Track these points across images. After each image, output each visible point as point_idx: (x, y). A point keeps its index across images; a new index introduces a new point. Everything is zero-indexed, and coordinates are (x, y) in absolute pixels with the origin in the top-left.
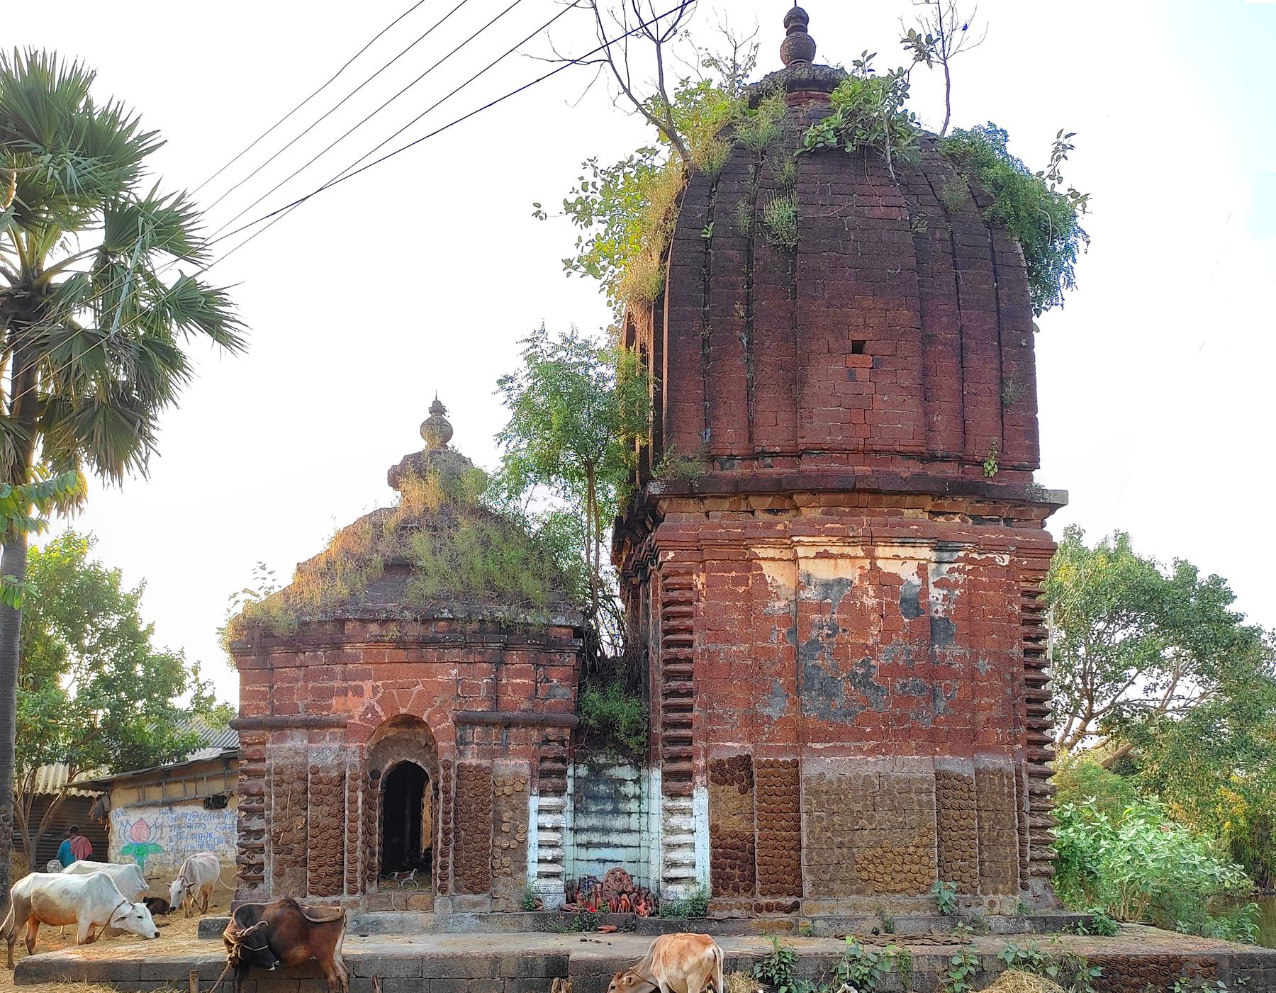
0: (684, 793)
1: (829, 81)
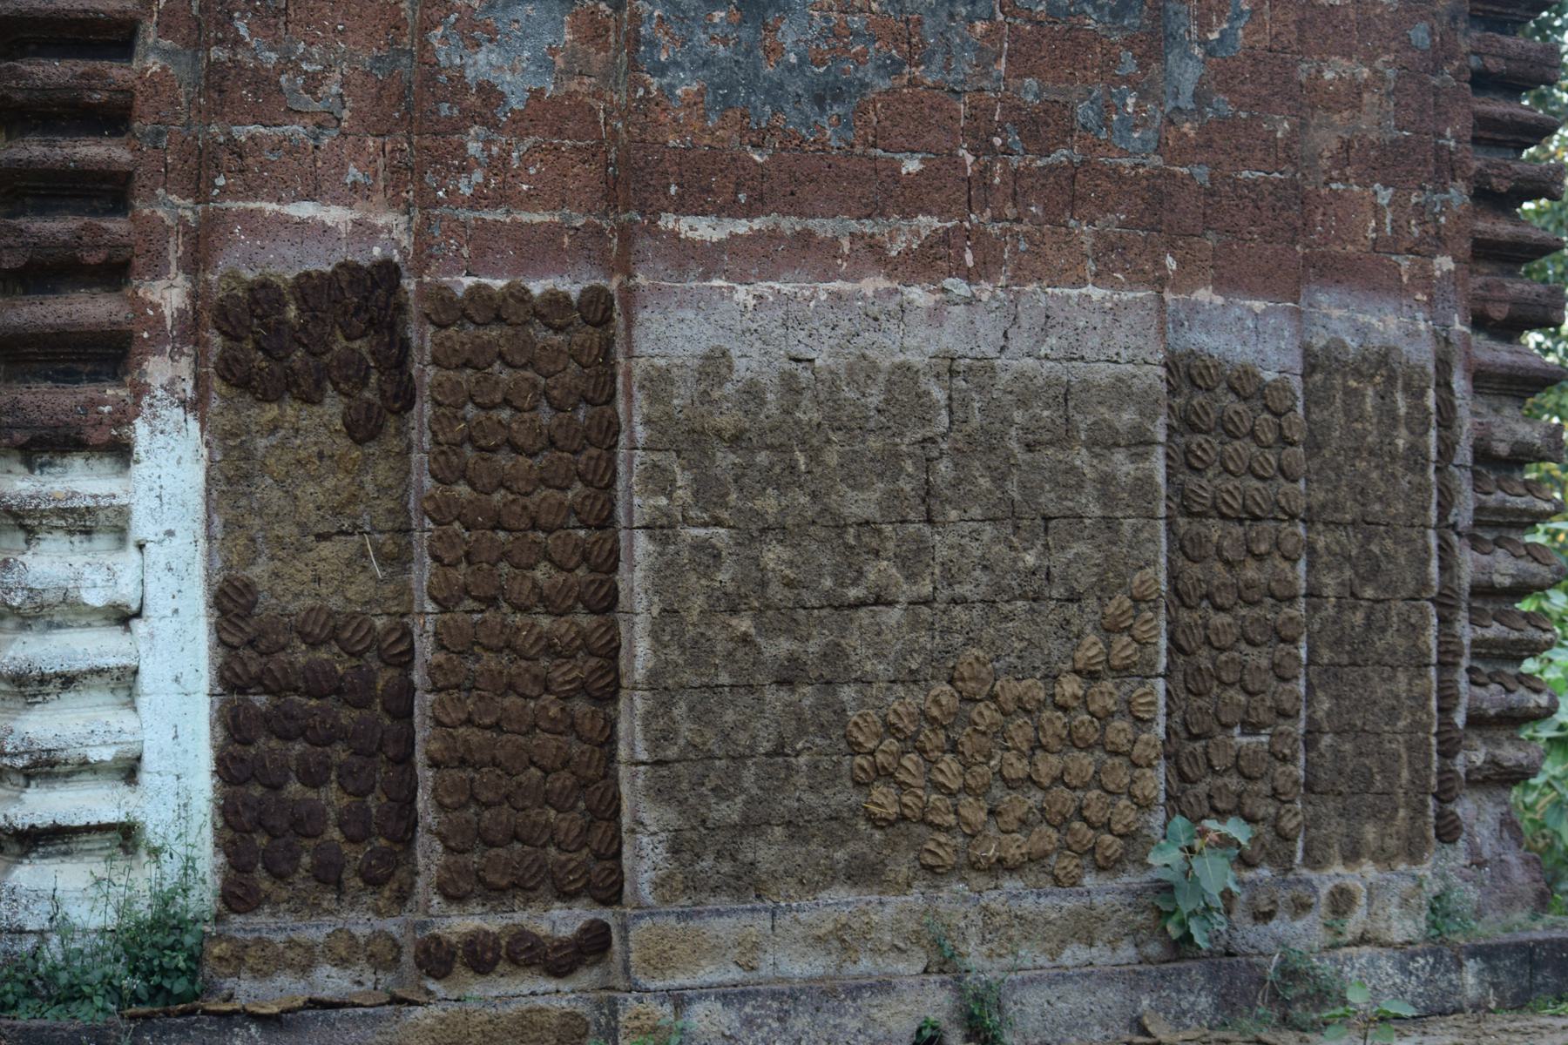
0: (95, 437)
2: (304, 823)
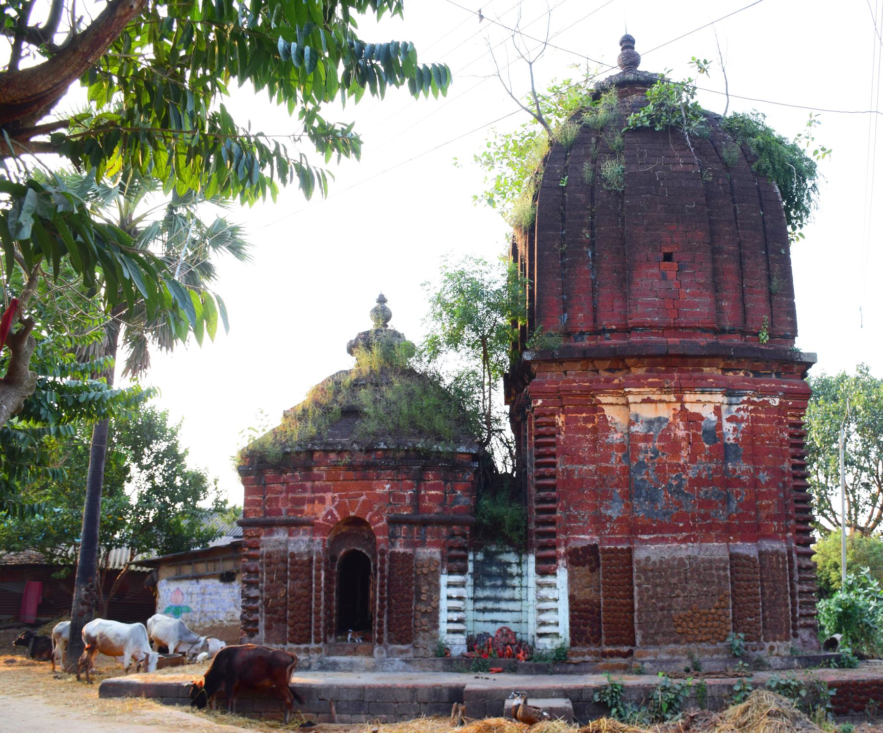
1: (649, 81)
2: (583, 633)
